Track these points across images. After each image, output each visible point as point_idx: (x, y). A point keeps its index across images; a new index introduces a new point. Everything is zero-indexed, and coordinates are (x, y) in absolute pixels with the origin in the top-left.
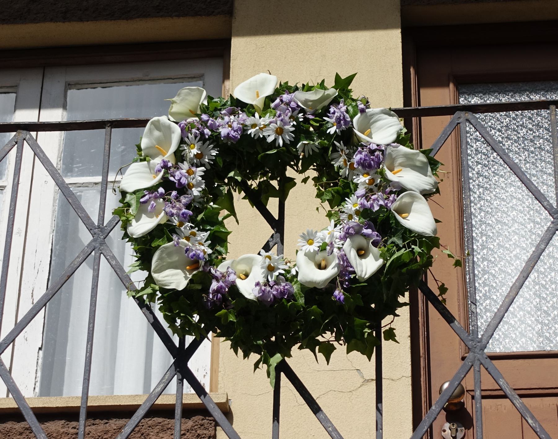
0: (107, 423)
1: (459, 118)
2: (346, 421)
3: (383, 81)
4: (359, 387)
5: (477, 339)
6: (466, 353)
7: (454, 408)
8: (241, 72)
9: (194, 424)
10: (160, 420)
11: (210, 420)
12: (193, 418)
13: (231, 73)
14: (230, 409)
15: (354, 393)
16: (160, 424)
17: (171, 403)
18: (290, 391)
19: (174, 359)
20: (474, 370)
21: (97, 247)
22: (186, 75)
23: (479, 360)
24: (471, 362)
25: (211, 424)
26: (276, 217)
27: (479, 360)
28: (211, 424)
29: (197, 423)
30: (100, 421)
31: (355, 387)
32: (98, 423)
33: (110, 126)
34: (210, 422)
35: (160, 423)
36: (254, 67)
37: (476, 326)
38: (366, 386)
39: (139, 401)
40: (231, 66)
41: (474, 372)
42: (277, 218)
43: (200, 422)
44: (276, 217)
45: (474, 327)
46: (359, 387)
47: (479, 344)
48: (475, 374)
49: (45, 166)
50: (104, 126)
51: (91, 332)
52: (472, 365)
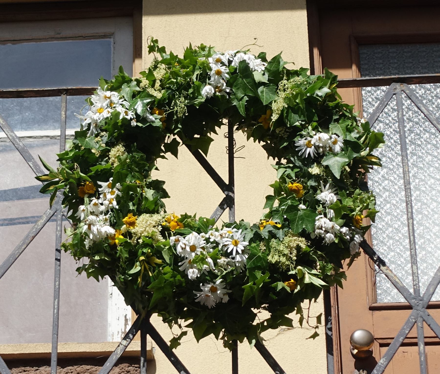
0: (37, 370)
1: (395, 89)
2: (265, 368)
3: (290, 42)
4: (277, 336)
5: (419, 298)
6: (373, 303)
7: (363, 356)
8: (152, 32)
9: (121, 371)
10: (88, 367)
11: (136, 367)
12: (120, 365)
13: (143, 32)
14: (154, 357)
15: (271, 341)
16: (88, 371)
17: (99, 351)
18: (211, 339)
19: (137, 315)
20: (417, 326)
21: (59, 209)
22: (97, 33)
23: (421, 317)
24: (415, 319)
25: (136, 370)
26: (227, 181)
27: (421, 317)
28: (136, 370)
29: (123, 370)
30: (31, 368)
31: (272, 335)
32: (28, 370)
33: (65, 94)
34: (136, 369)
35: (88, 370)
36: (165, 27)
37: (418, 286)
38: (282, 335)
39: (68, 349)
40: (143, 26)
41: (417, 328)
42: (227, 183)
43: (126, 369)
44: (227, 181)
45: (416, 287)
46: (277, 336)
47: (421, 302)
48: (418, 330)
49: (6, 131)
50: (60, 94)
51: (57, 290)
52: (416, 322)
